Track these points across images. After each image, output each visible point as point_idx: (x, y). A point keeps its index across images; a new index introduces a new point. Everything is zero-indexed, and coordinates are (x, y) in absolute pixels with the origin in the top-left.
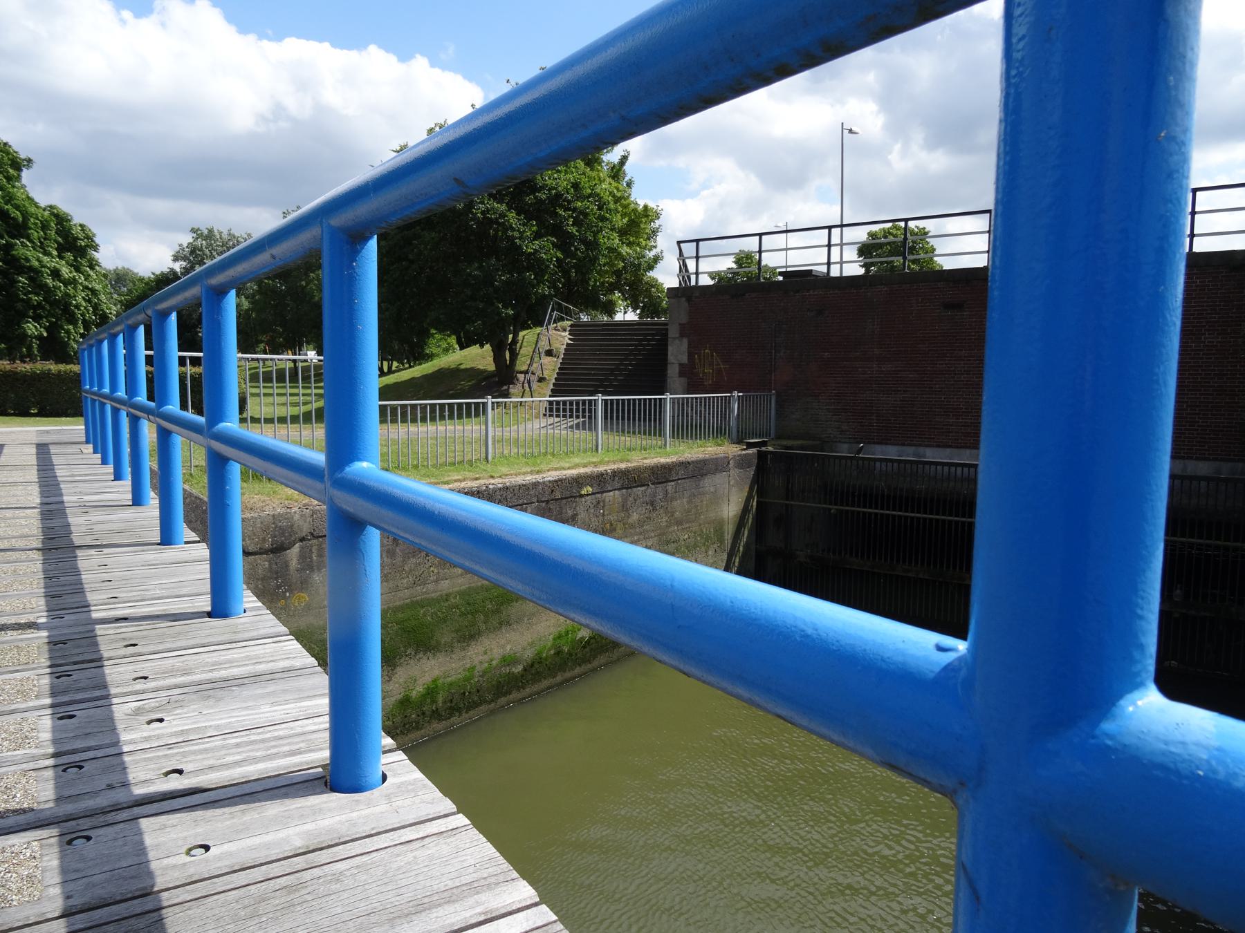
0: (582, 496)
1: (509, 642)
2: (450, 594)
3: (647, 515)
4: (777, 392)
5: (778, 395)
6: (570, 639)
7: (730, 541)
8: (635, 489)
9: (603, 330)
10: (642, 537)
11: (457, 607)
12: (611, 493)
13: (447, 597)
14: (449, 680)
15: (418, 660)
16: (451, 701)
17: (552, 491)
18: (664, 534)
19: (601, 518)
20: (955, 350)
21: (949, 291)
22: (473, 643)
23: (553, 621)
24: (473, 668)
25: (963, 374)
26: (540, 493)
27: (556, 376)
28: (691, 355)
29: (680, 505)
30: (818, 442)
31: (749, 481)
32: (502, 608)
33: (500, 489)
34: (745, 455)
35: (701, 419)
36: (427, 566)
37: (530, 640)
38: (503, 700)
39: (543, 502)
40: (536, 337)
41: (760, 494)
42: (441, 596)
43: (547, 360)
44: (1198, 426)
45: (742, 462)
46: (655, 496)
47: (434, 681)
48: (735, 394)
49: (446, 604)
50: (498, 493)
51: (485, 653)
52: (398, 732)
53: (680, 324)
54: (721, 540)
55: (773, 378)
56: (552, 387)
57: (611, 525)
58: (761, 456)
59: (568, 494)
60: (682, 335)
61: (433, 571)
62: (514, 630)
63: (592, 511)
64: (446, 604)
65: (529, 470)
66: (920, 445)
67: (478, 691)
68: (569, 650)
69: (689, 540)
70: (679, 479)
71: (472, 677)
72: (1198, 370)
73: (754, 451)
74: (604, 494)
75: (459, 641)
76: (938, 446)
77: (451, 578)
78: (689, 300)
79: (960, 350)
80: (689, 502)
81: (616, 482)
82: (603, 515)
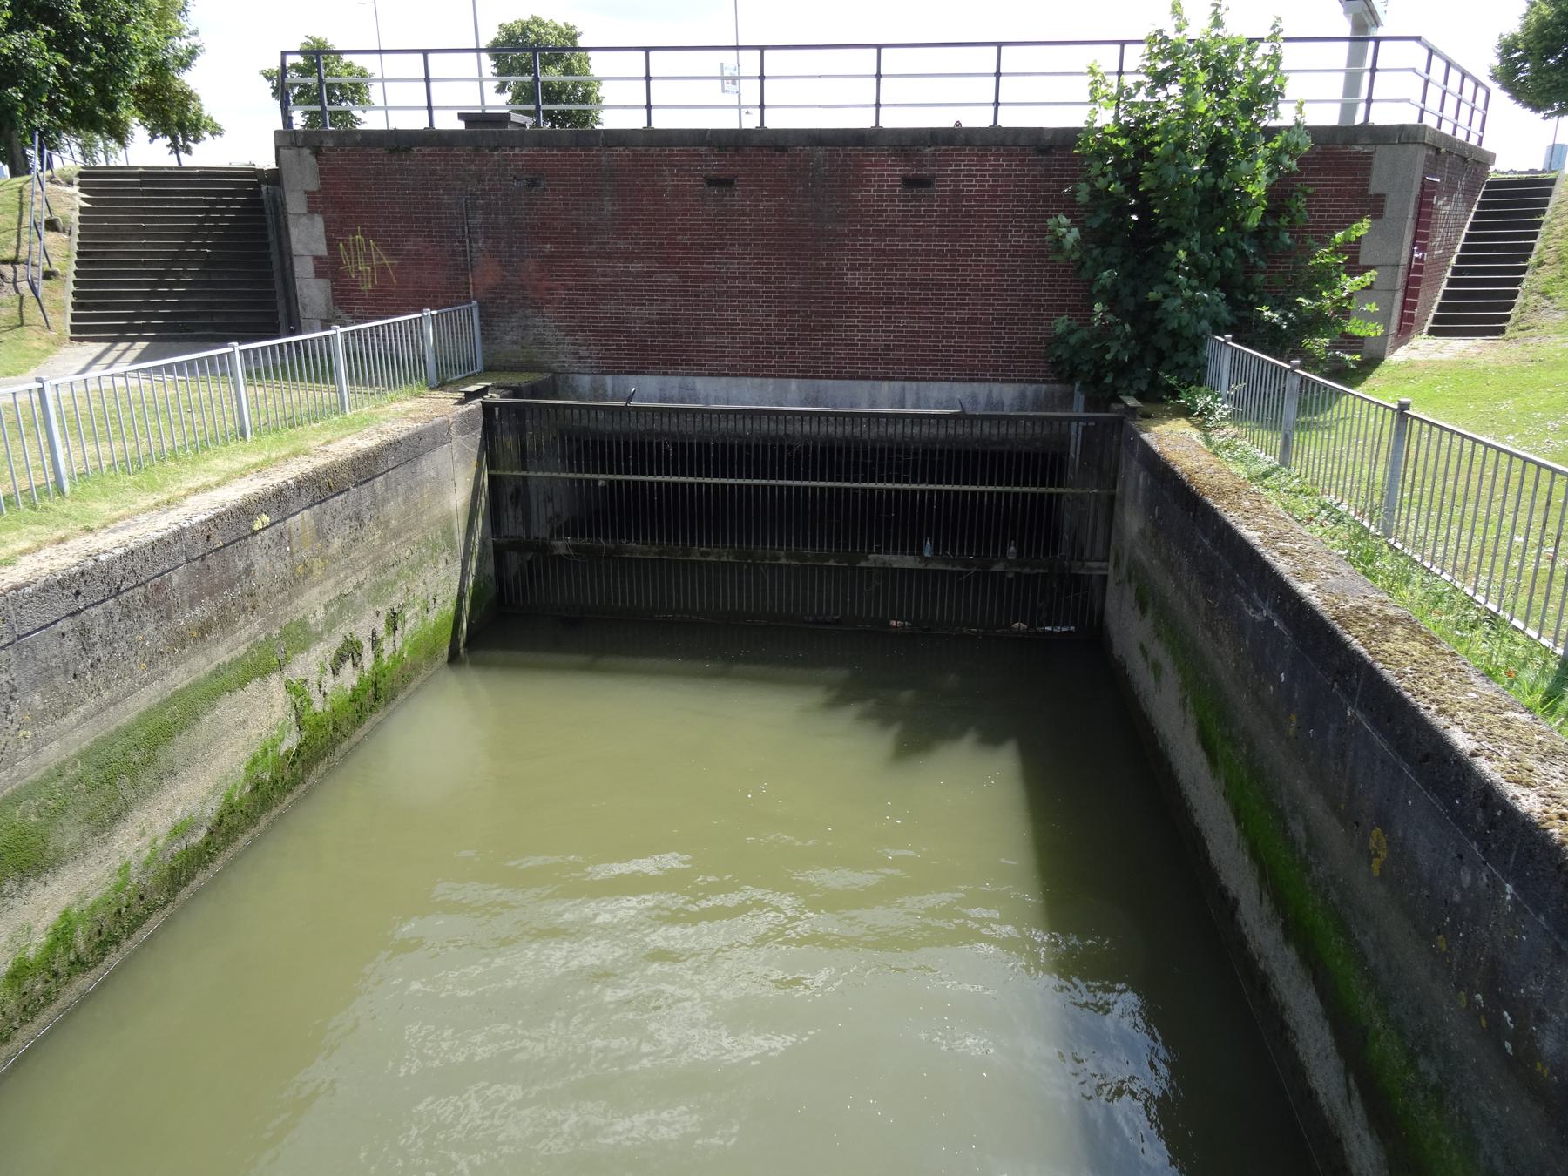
0: (255, 533)
1: (177, 801)
2: (64, 763)
3: (352, 536)
4: (479, 302)
5: (481, 306)
6: (270, 761)
7: (462, 543)
8: (330, 501)
9: (142, 184)
10: (350, 571)
11: (80, 780)
12: (298, 517)
13: (60, 770)
14: (89, 902)
15: (29, 894)
16: (100, 933)
17: (209, 537)
18: (379, 557)
19: (288, 559)
20: (726, 244)
21: (714, 160)
22: (120, 827)
23: (241, 742)
24: (127, 866)
25: (738, 278)
26: (190, 547)
27: (74, 268)
28: (331, 243)
29: (394, 507)
30: (549, 375)
31: (475, 451)
32: (157, 753)
33: (120, 558)
34: (467, 413)
35: (360, 344)
36: (11, 731)
37: (211, 785)
38: (184, 893)
39: (196, 559)
40: (17, 195)
41: (491, 465)
42: (48, 772)
43: (50, 237)
44: (1004, 343)
45: (465, 424)
46: (360, 504)
47: (65, 915)
48: (428, 312)
49: (61, 783)
50: (117, 566)
51: (143, 834)
52: (16, 1024)
53: (306, 192)
54: (451, 545)
55: (471, 281)
56: (72, 288)
57: (305, 565)
58: (487, 408)
59: (233, 535)
60: (312, 210)
61: (25, 737)
62: (183, 780)
63: (274, 552)
64: (61, 783)
65: (152, 502)
66: (688, 375)
67: (142, 898)
68: (271, 777)
69: (412, 557)
70: (389, 470)
71: (127, 880)
72: (1065, 300)
73: (475, 404)
74: (289, 521)
75: (95, 834)
76: (711, 375)
77: (60, 736)
78: (317, 152)
79: (731, 245)
80: (406, 500)
81: (303, 497)
82: (291, 553)
